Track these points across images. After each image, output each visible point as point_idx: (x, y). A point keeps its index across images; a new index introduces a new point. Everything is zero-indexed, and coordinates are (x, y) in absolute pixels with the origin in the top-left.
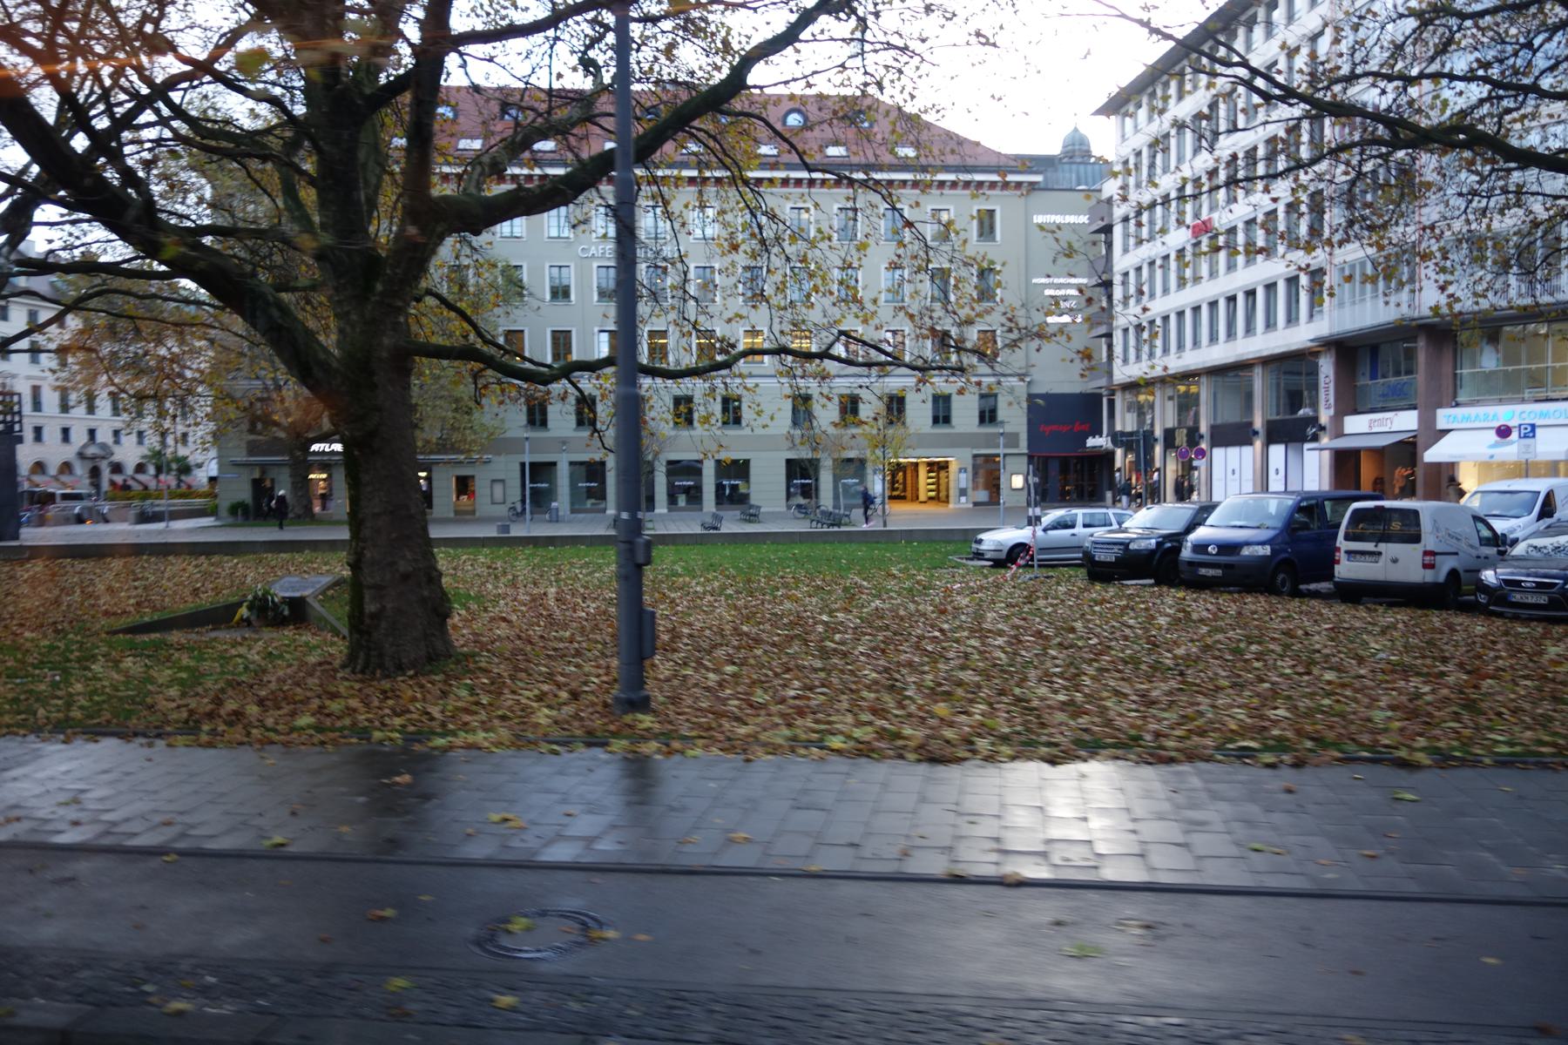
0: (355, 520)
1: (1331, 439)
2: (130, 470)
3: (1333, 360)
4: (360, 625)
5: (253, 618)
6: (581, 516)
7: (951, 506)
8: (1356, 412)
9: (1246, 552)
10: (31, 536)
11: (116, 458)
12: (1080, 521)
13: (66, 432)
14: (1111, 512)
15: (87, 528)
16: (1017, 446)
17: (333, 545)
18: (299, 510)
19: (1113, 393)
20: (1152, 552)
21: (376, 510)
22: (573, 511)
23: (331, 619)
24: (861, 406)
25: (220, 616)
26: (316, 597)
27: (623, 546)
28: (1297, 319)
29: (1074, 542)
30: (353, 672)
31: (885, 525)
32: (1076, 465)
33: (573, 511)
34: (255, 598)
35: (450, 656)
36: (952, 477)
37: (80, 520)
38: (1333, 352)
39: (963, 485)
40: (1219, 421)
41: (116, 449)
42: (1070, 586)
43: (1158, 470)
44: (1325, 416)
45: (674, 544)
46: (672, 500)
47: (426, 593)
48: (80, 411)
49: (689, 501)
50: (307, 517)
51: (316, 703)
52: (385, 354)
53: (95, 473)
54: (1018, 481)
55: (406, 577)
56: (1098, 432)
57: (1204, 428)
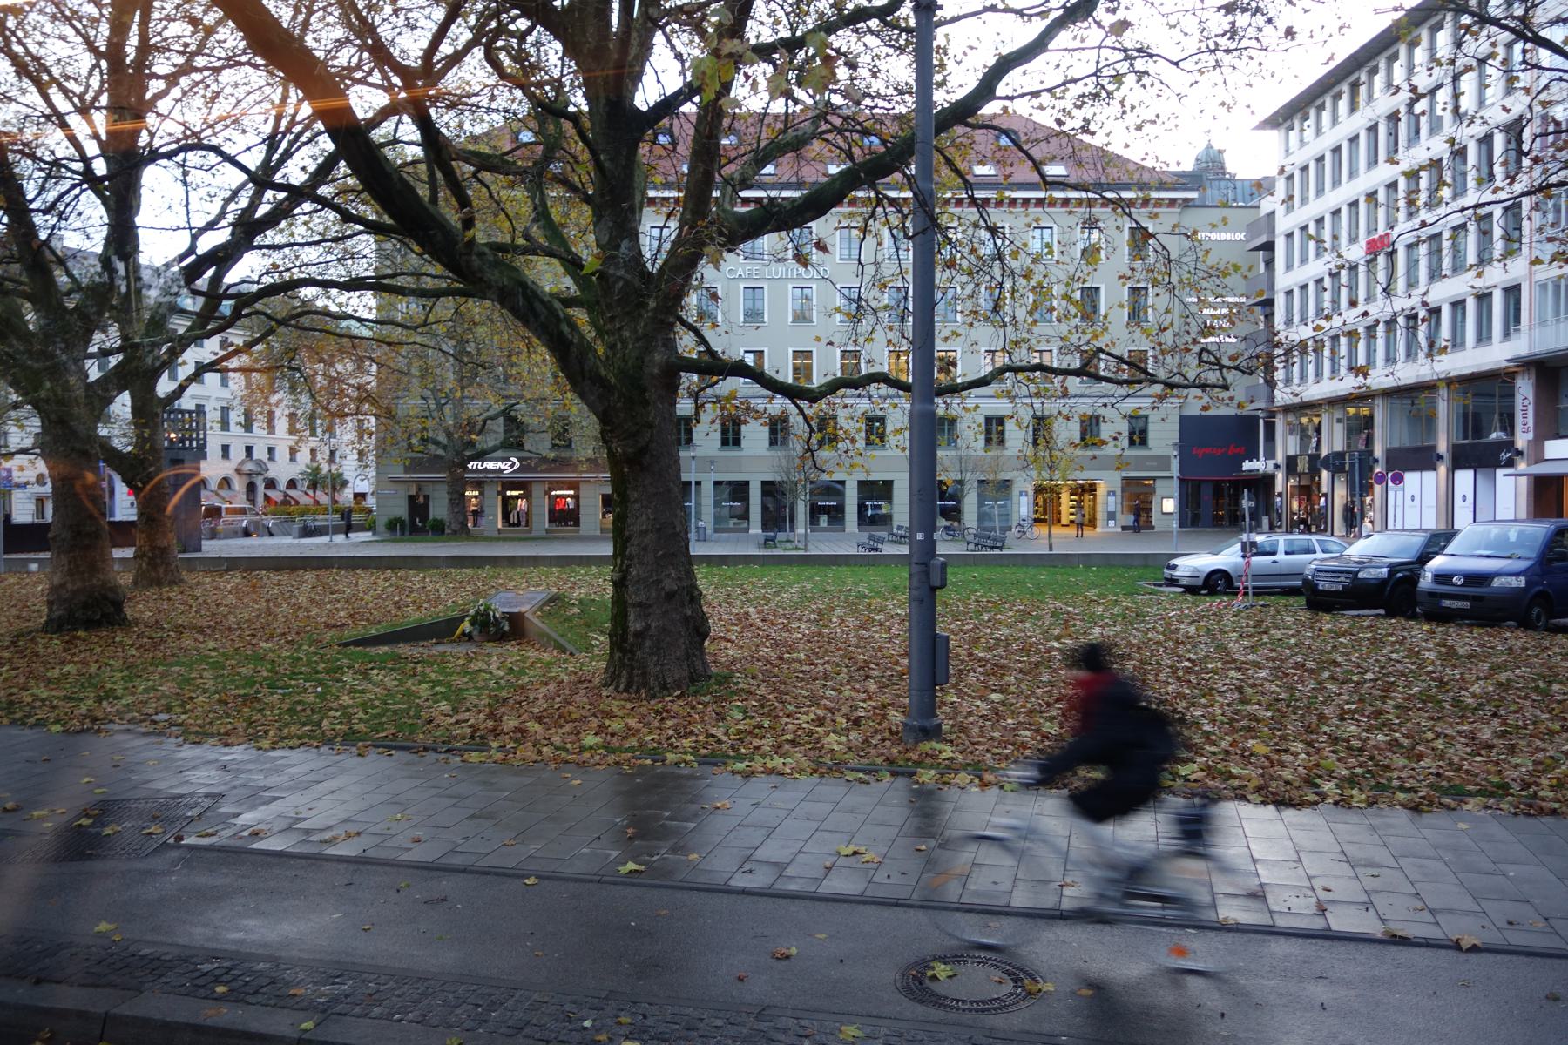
0: (620, 535)
1: (1528, 465)
2: (282, 485)
3: (1534, 377)
4: (621, 641)
5: (475, 633)
6: (725, 535)
7: (1098, 530)
8: (1558, 436)
9: (1497, 583)
10: (211, 548)
11: (270, 474)
12: (1281, 548)
13: (225, 450)
14: (1314, 538)
15: (253, 541)
16: (1168, 469)
17: (599, 560)
18: (455, 526)
19: (1272, 414)
20: (1382, 583)
21: (644, 528)
22: (716, 531)
24: (1102, 426)
25: (442, 630)
27: (916, 569)
28: (1490, 338)
29: (1275, 569)
30: (616, 689)
31: (1051, 549)
32: (1229, 488)
33: (716, 531)
34: (477, 612)
35: (710, 677)
36: (1100, 500)
37: (247, 533)
38: (1533, 372)
39: (1112, 509)
40: (1396, 445)
41: (270, 465)
42: (1294, 614)
43: (1325, 495)
44: (1522, 440)
45: (847, 565)
46: (814, 520)
47: (689, 613)
48: (236, 430)
49: (830, 521)
50: (462, 533)
51: (594, 722)
52: (656, 371)
53: (251, 488)
54: (1170, 505)
55: (670, 596)
56: (1254, 455)
57: (1378, 452)
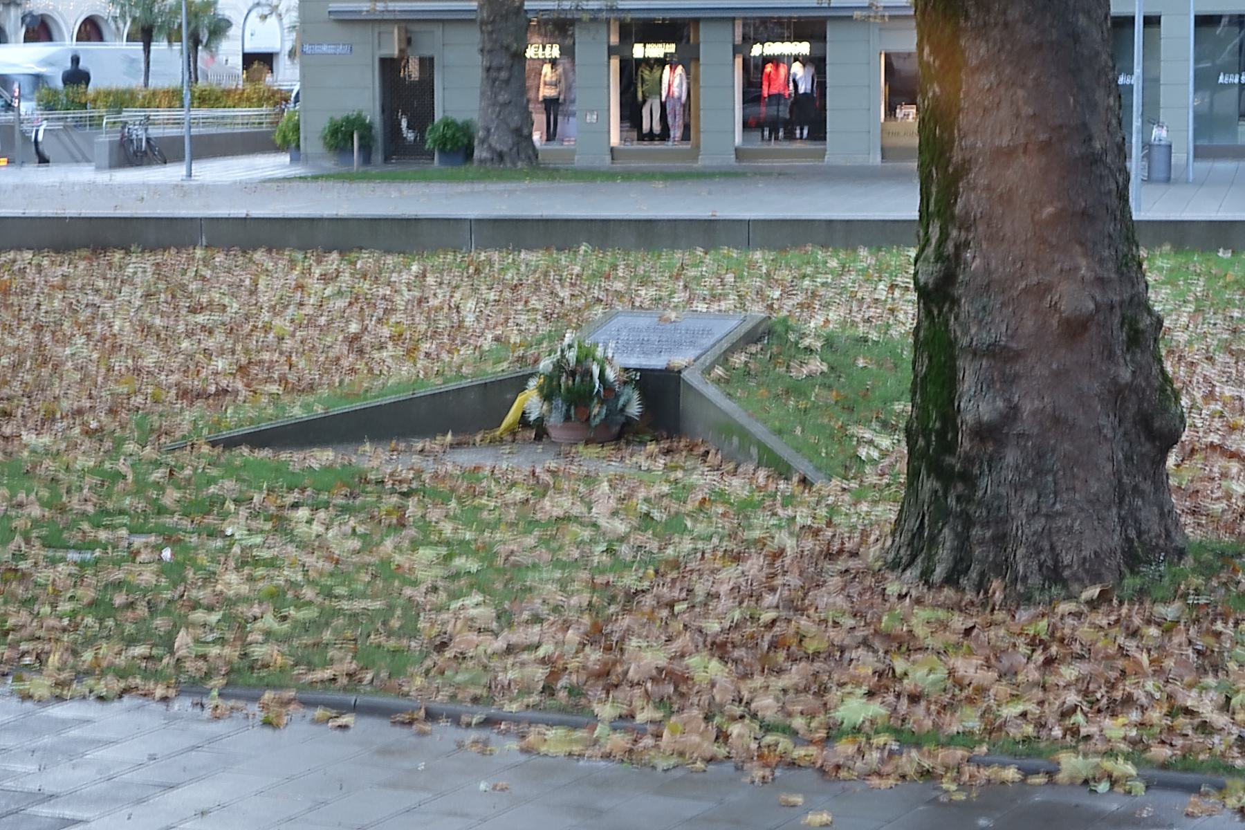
5: (554, 421)
6: (1224, 166)
18: (500, 141)
21: (1004, 141)
22: (1199, 153)
23: (758, 430)
26: (708, 371)
33: (1199, 153)
34: (559, 366)
35: (1181, 553)
47: (1125, 375)
55: (1075, 328)
